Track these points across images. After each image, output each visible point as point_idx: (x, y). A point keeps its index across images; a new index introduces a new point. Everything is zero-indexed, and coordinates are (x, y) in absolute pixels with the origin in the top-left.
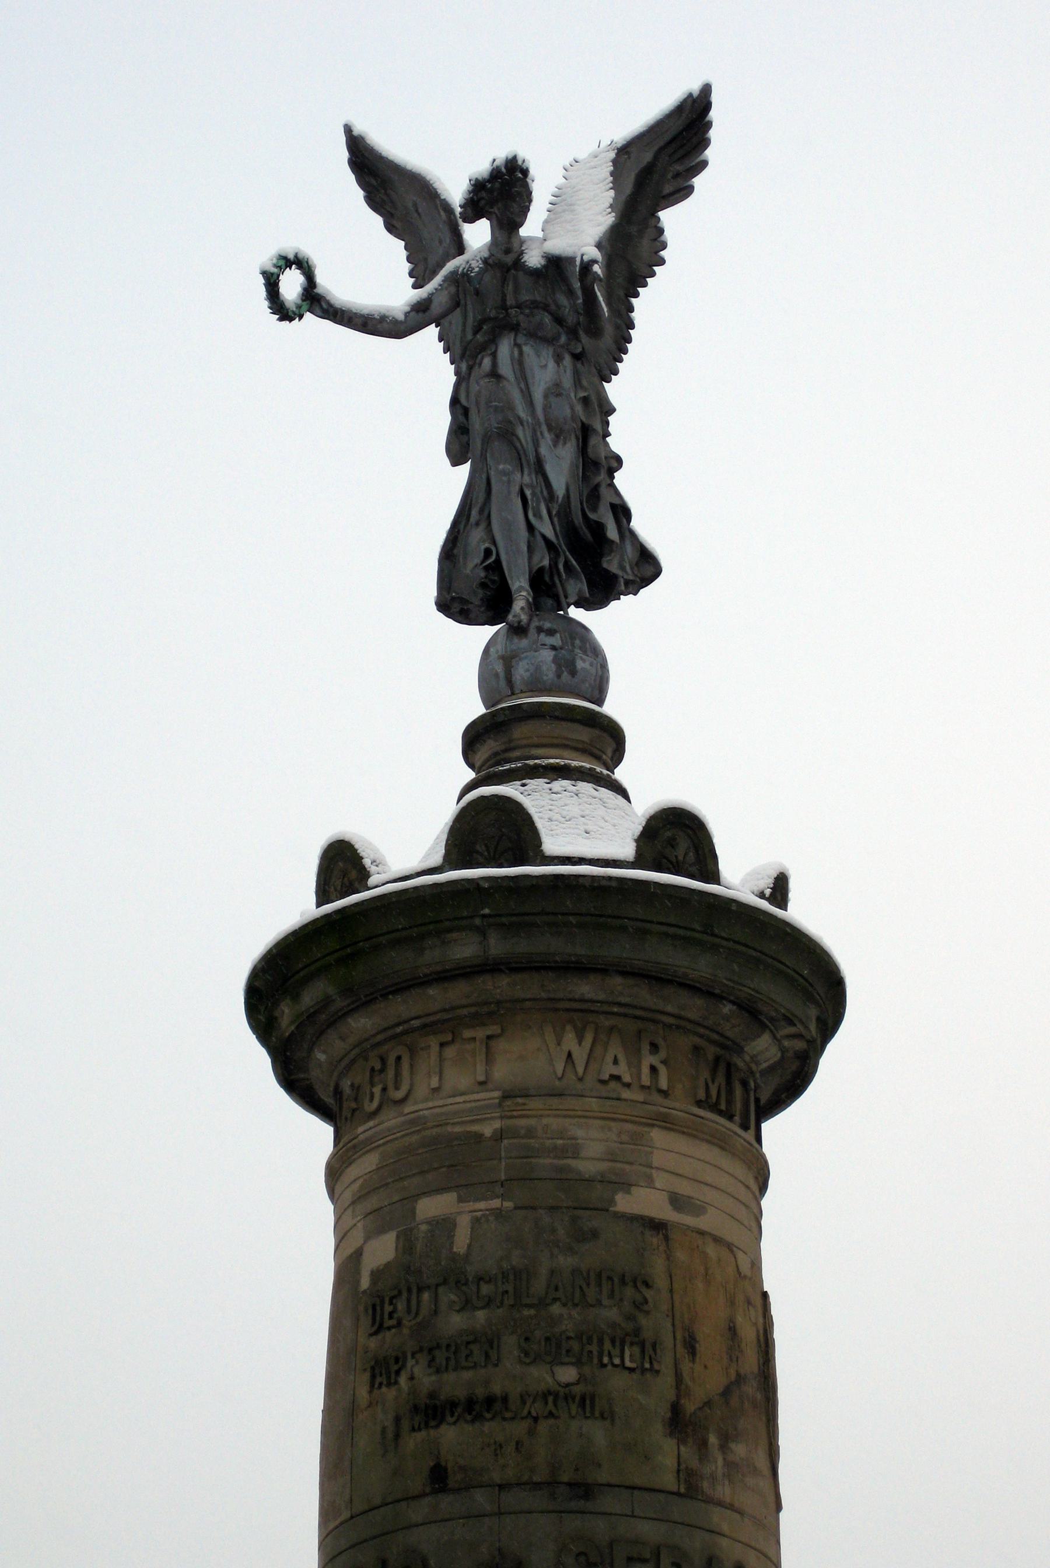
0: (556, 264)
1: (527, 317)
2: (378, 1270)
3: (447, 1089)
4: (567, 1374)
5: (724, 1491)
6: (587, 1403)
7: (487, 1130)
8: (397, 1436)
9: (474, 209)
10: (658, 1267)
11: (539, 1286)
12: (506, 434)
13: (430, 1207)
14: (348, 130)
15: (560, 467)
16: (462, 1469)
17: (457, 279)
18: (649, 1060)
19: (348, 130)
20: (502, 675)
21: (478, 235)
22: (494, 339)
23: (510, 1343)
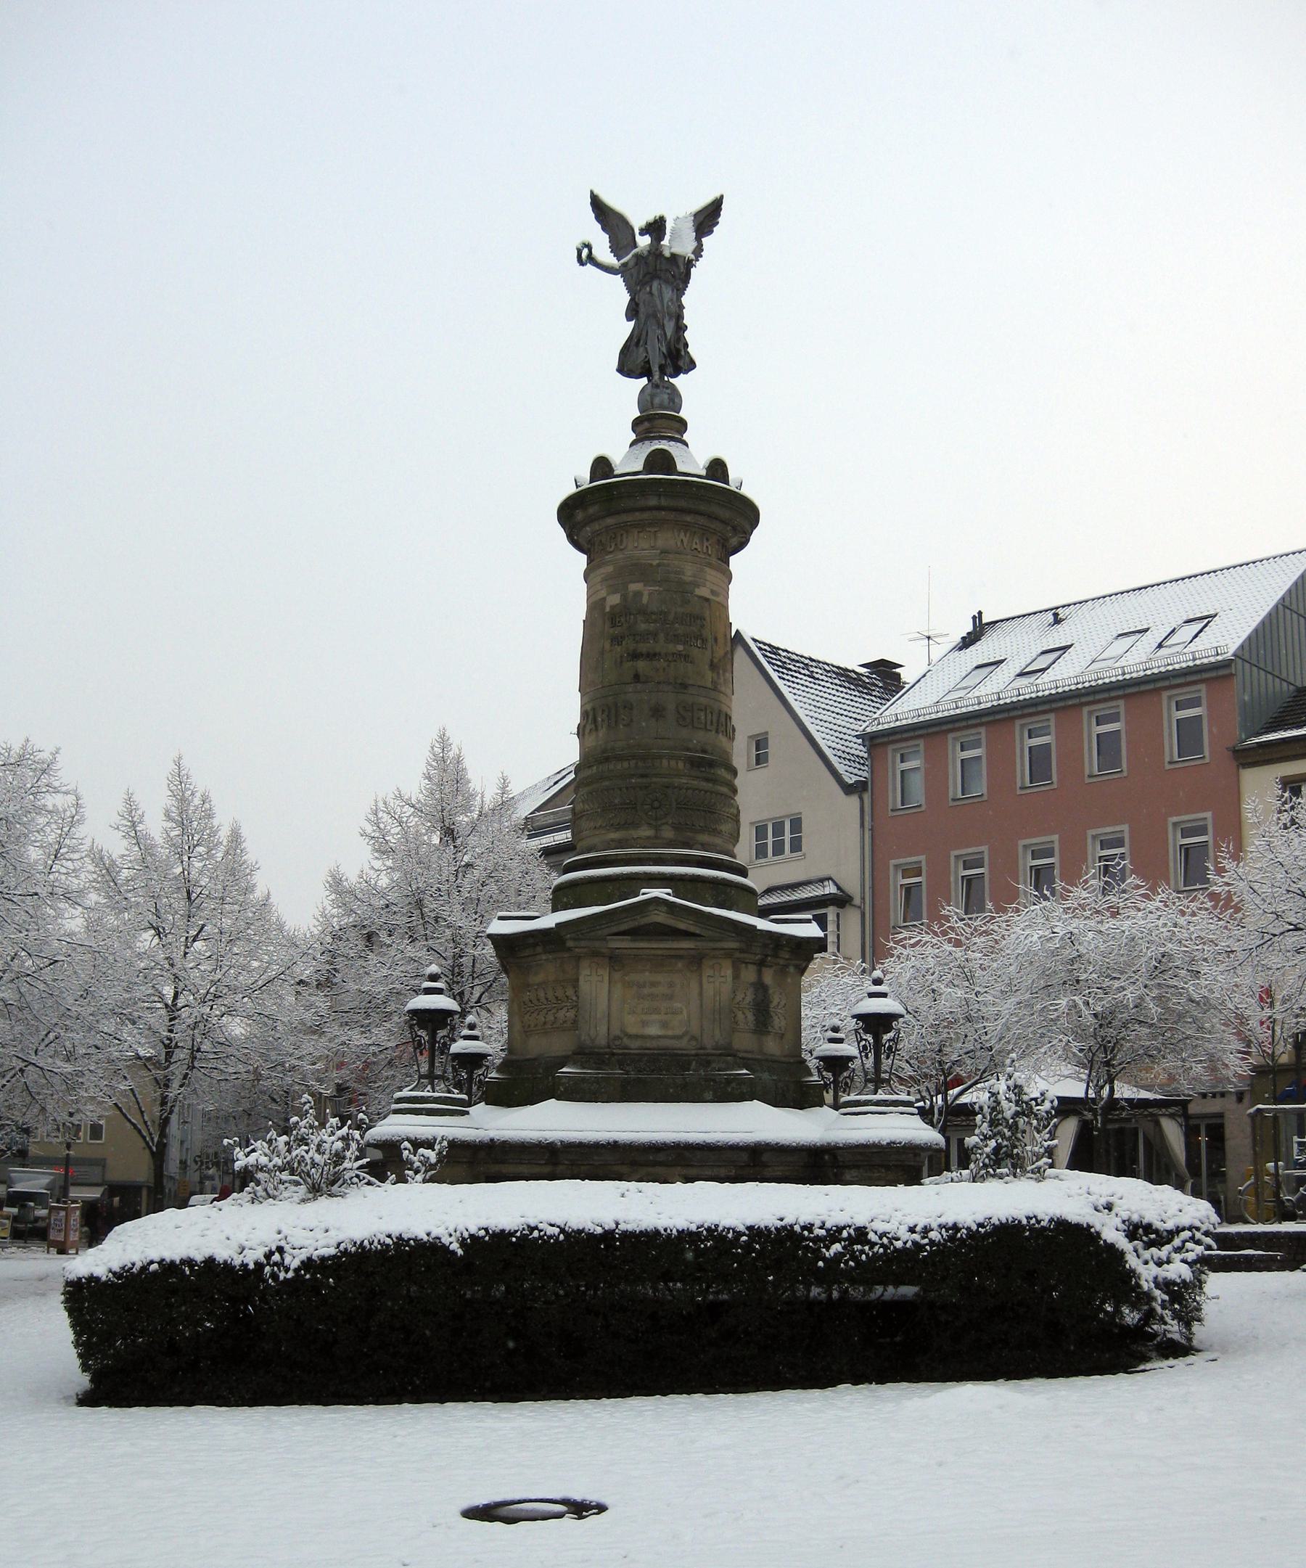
0: (674, 256)
1: (654, 273)
3: (641, 547)
4: (680, 648)
5: (723, 689)
6: (686, 657)
7: (655, 563)
9: (643, 232)
10: (707, 614)
11: (671, 617)
12: (655, 316)
13: (634, 587)
14: (592, 192)
15: (670, 328)
17: (637, 256)
18: (706, 544)
19: (592, 192)
21: (644, 242)
22: (652, 279)
23: (662, 635)
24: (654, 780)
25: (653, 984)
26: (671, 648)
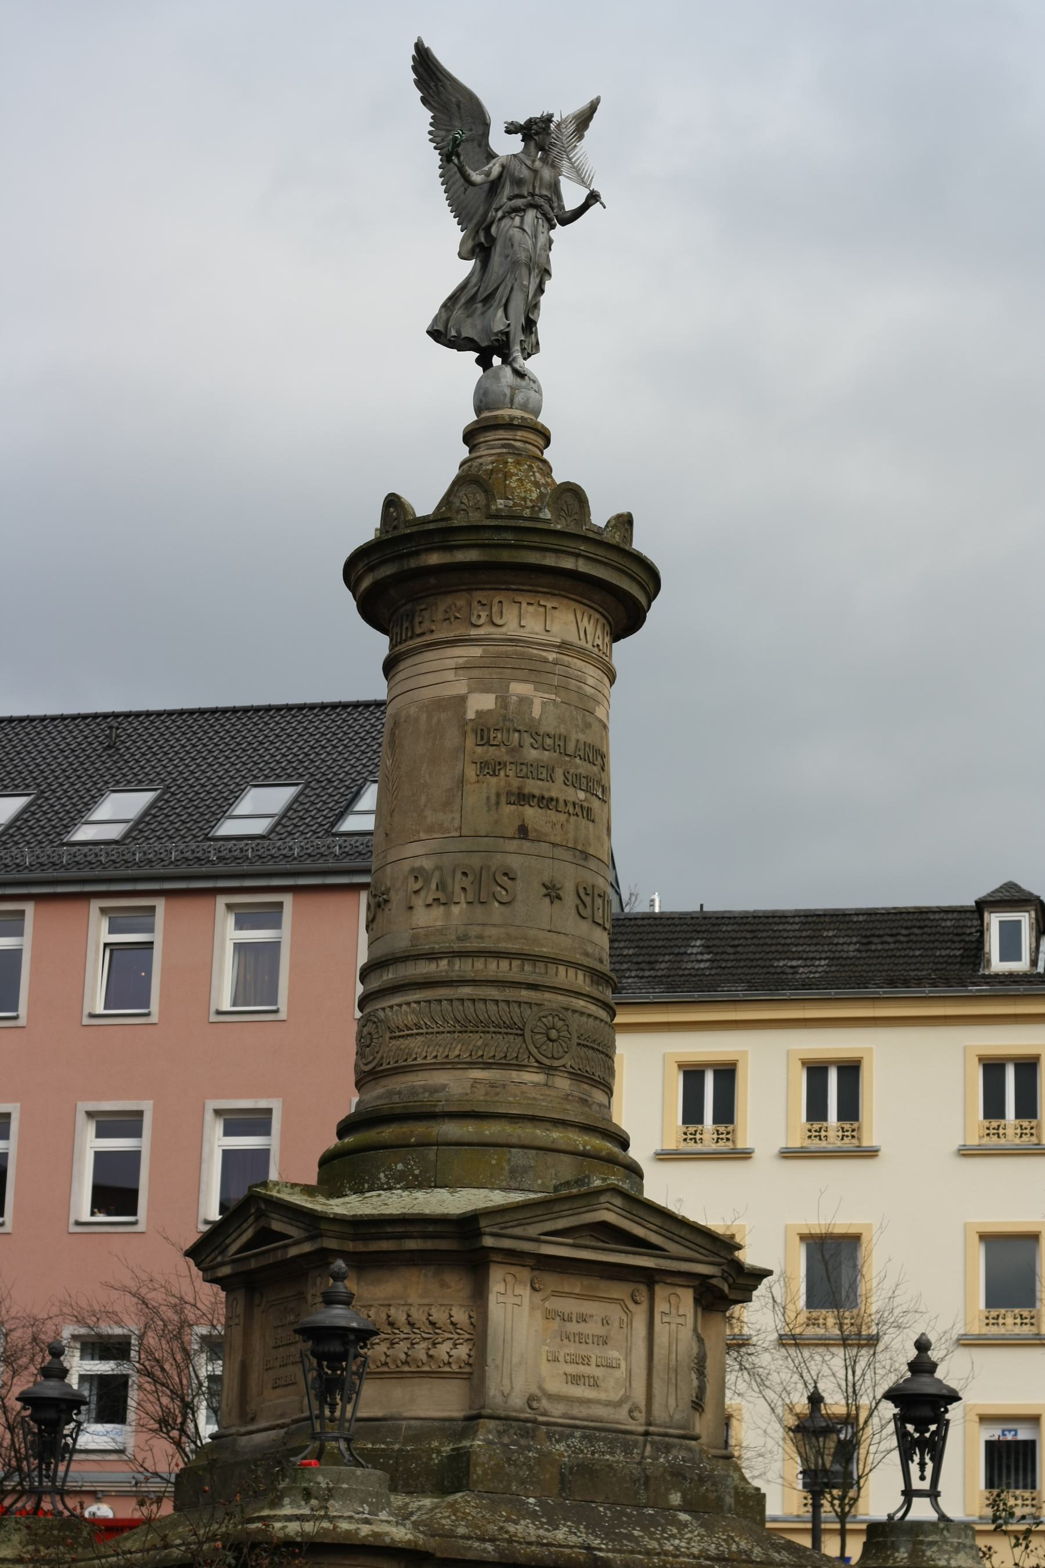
1: (506, 189)
2: (482, 711)
8: (498, 803)
9: (512, 129)
16: (536, 830)
20: (508, 396)
24: (547, 995)
25: (583, 1319)
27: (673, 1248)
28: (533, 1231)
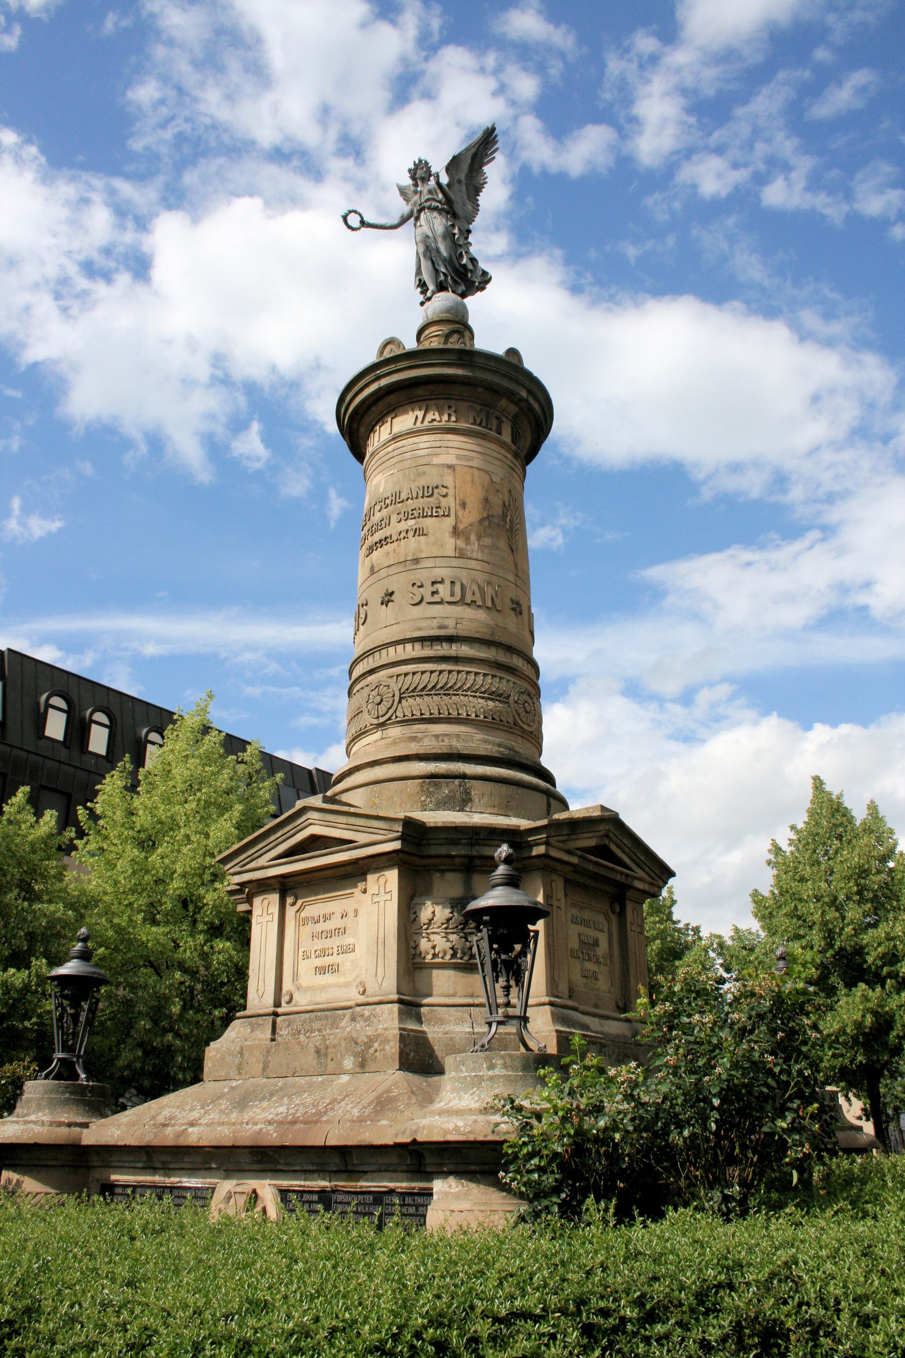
26: (403, 526)
27: (362, 838)
28: (262, 861)
